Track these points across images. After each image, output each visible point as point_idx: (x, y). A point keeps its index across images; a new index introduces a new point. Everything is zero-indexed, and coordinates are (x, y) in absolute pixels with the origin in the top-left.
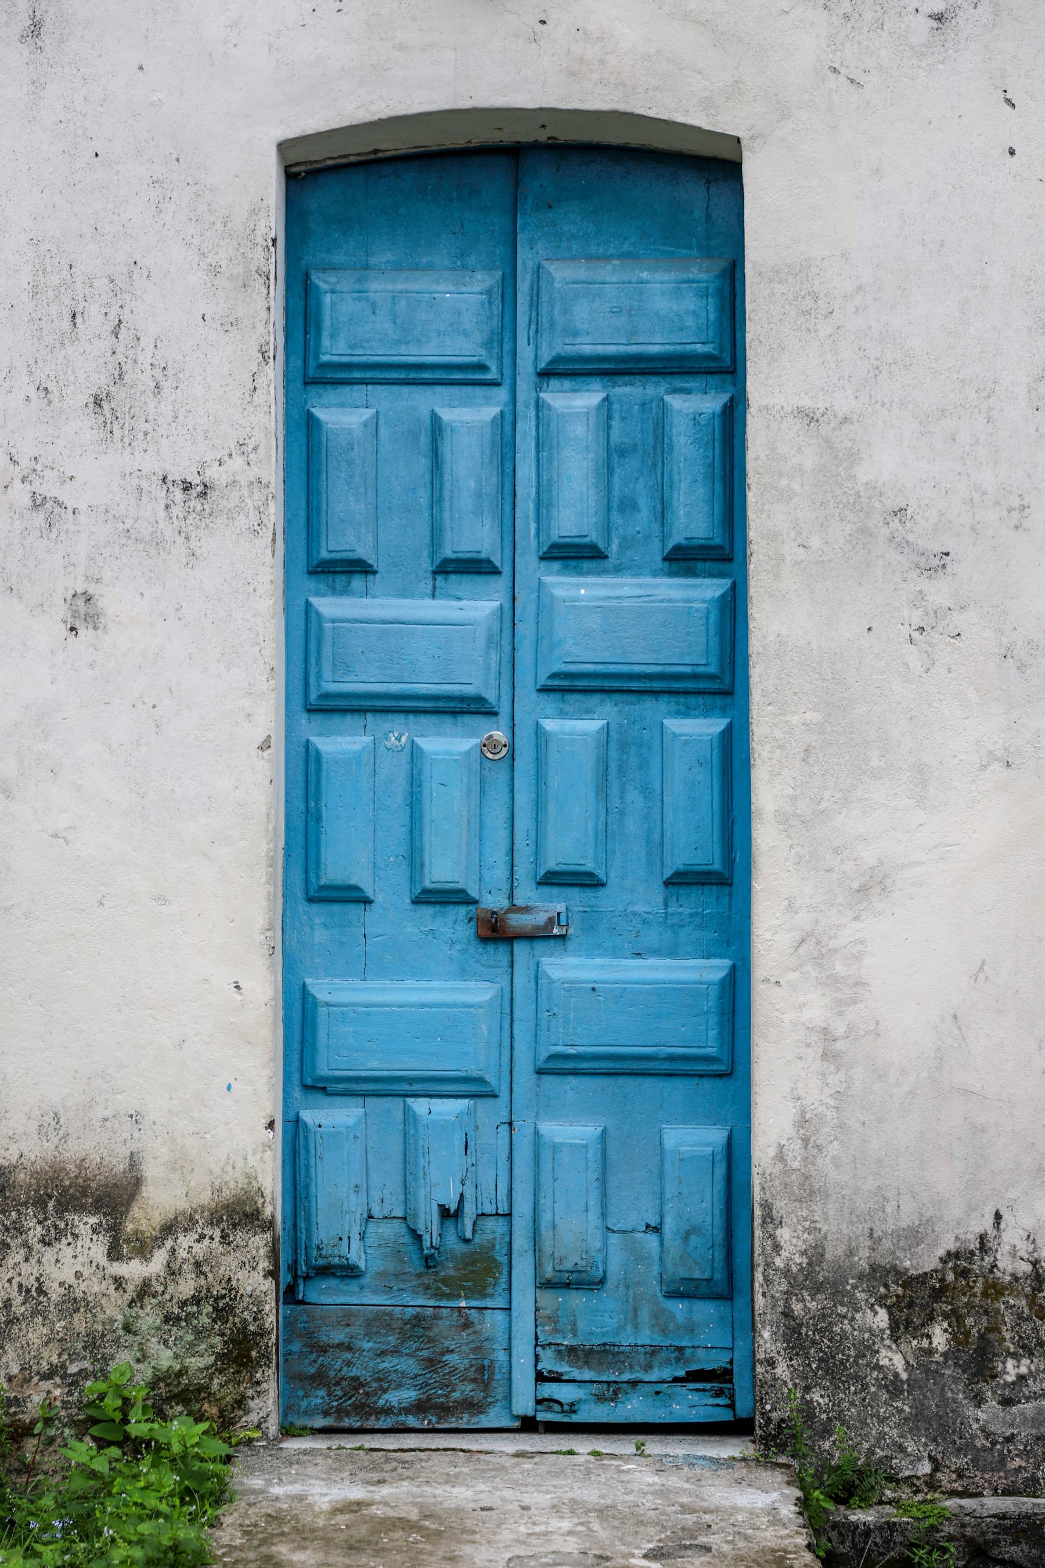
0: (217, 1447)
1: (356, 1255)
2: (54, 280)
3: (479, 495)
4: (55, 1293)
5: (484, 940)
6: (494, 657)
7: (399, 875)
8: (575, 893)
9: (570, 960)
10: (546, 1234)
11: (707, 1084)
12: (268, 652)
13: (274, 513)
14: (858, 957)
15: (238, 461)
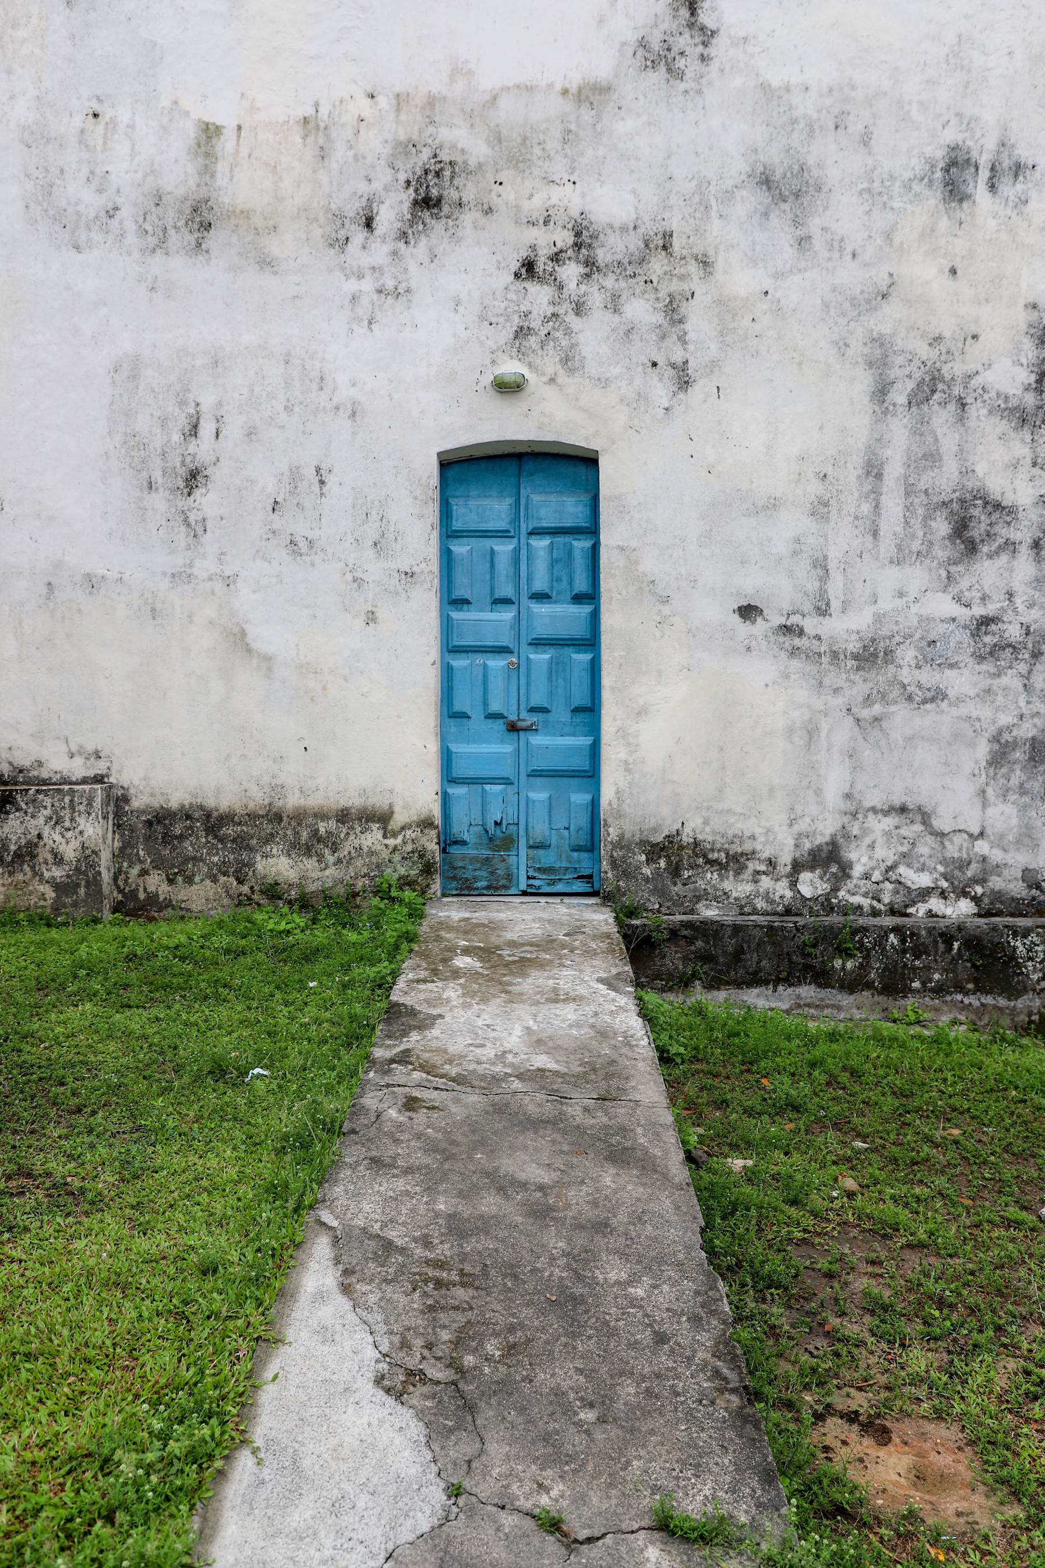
0: (421, 900)
1: (466, 837)
2: (360, 502)
3: (507, 576)
4: (365, 849)
5: (509, 731)
6: (513, 633)
7: (480, 708)
8: (540, 714)
9: (539, 738)
10: (530, 829)
11: (585, 780)
12: (435, 631)
13: (436, 582)
14: (637, 736)
15: (424, 564)
